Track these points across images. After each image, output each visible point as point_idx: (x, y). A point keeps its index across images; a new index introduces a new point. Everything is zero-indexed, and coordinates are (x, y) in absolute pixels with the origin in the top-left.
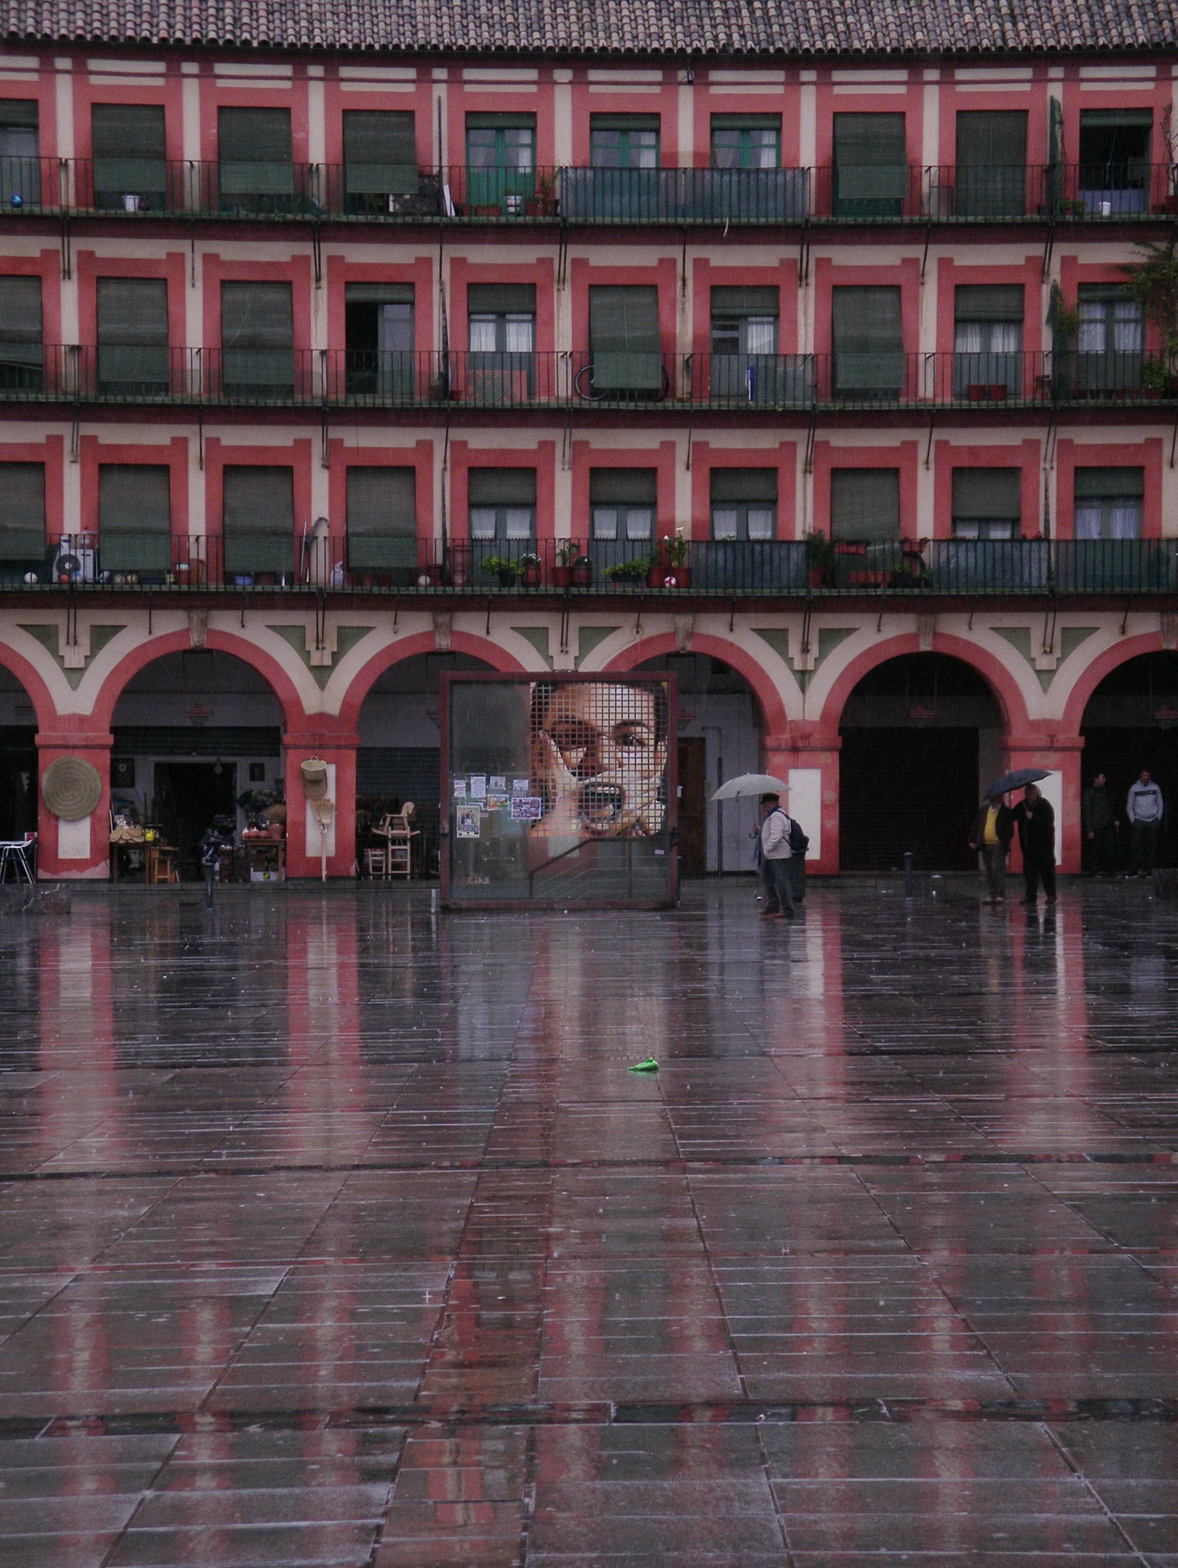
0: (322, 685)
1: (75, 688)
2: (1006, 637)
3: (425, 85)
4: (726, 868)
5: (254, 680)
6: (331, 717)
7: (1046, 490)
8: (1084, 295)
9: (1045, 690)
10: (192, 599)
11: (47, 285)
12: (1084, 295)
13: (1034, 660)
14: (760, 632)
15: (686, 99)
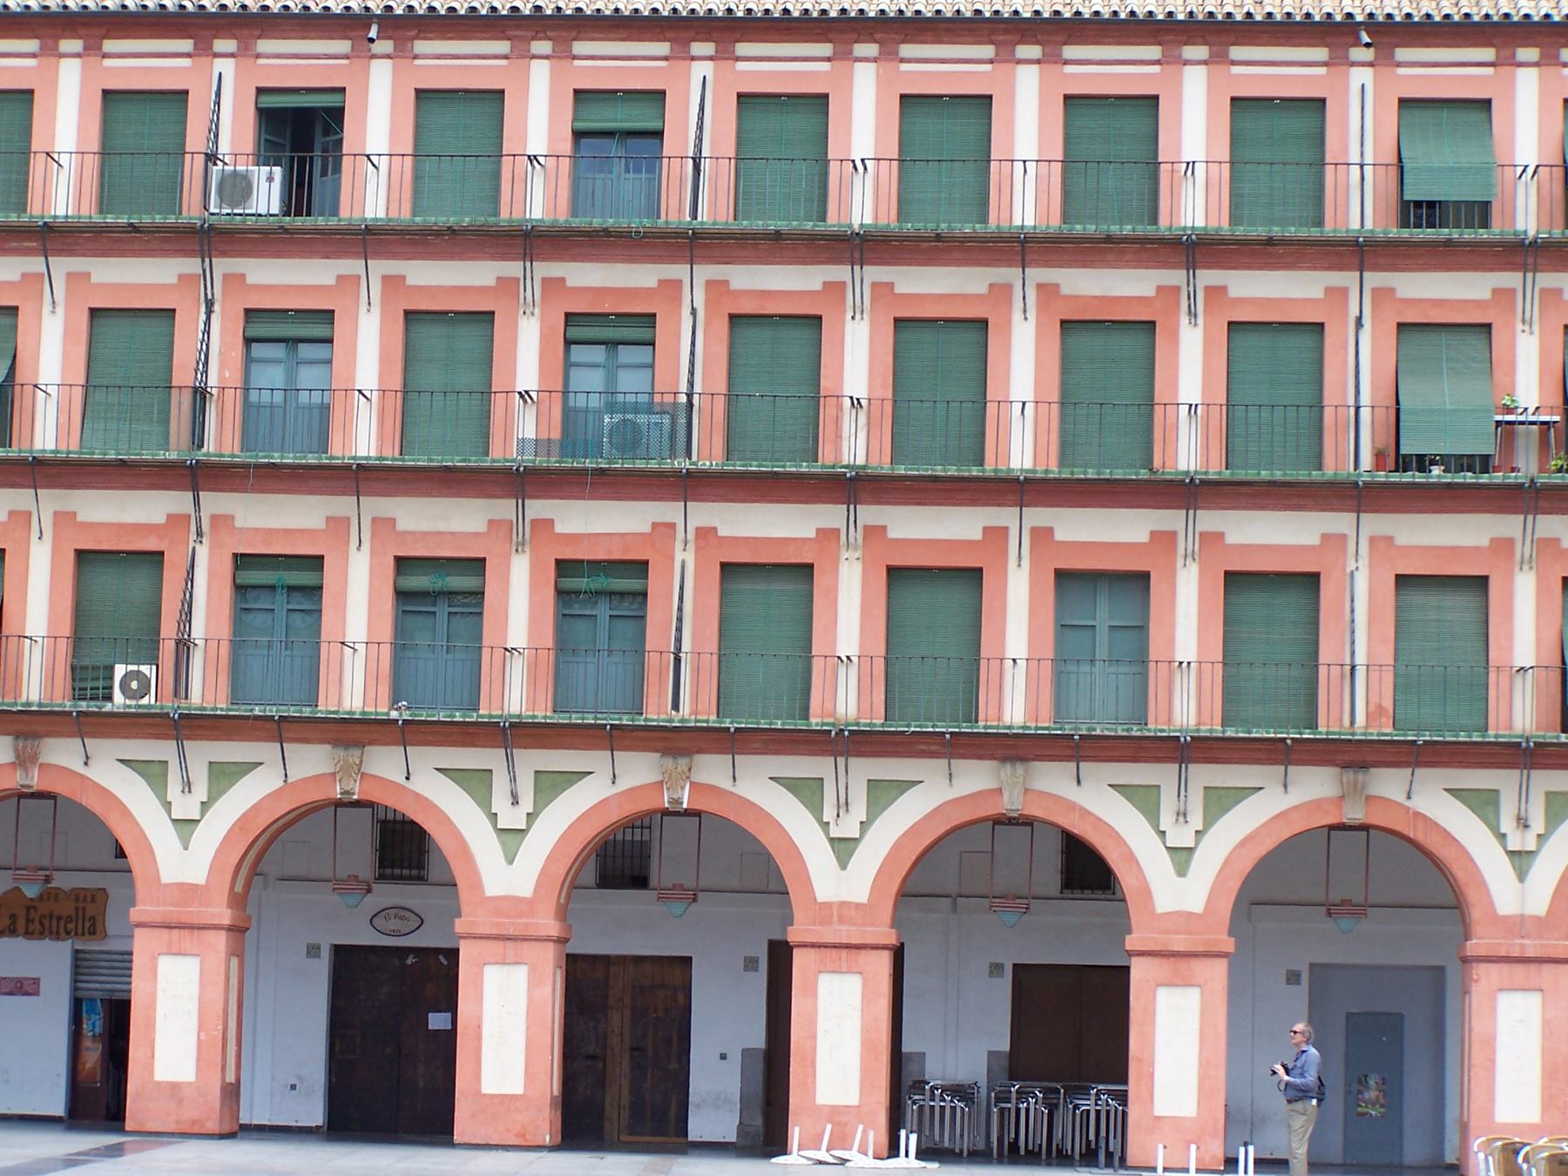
0: (1182, 871)
5: (1439, 890)
7: (682, 588)
9: (843, 866)
10: (677, 741)
13: (1504, 835)
15: (540, 74)
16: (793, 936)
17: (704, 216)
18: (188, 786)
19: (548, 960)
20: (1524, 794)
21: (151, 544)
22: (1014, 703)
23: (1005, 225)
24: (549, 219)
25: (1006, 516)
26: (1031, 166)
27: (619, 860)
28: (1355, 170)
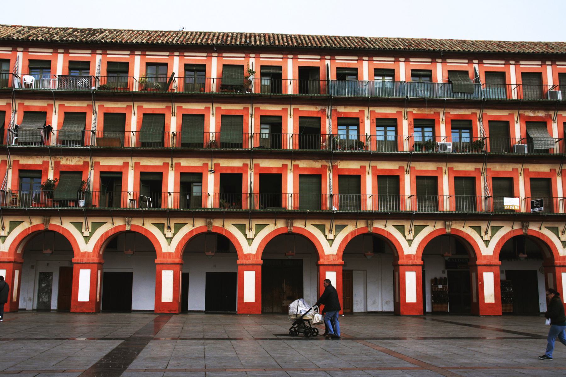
0: (250, 245)
2: (238, 228)
3: (15, 52)
4: (370, 309)
9: (87, 243)
10: (209, 215)
11: (548, 126)
20: (250, 224)
21: (200, 171)
23: (208, 92)
25: (366, 164)
26: (215, 80)
27: (112, 244)
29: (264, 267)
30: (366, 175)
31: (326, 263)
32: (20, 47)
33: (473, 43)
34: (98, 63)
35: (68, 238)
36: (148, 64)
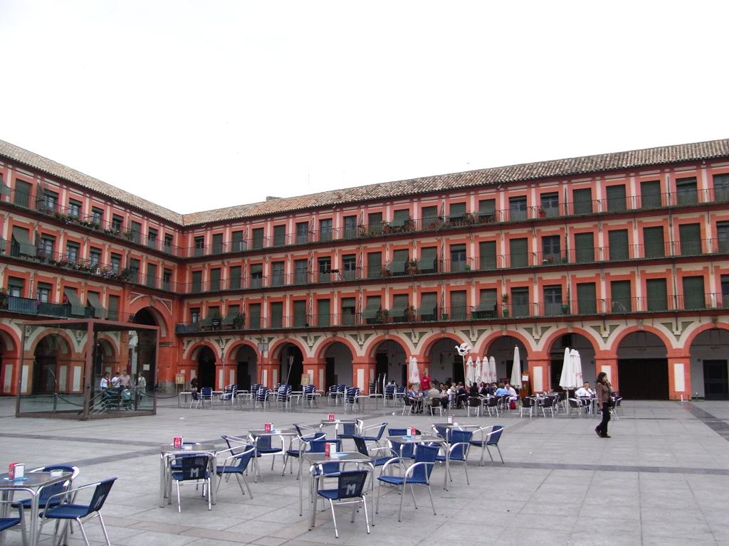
0: (605, 342)
1: (678, 340)
5: (660, 343)
6: (608, 351)
8: (694, 181)
10: (640, 316)
12: (694, 181)
14: (351, 335)
16: (668, 356)
17: (568, 214)
18: (415, 337)
19: (615, 362)
20: (536, 328)
21: (701, 274)
22: (640, 306)
24: (709, 201)
25: (634, 269)
28: (668, 195)
29: (238, 366)
30: (708, 275)
31: (672, 356)
32: (598, 176)
33: (121, 191)
34: (566, 192)
35: (402, 345)
36: (715, 176)
